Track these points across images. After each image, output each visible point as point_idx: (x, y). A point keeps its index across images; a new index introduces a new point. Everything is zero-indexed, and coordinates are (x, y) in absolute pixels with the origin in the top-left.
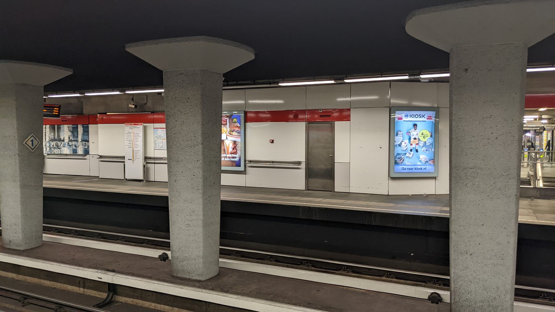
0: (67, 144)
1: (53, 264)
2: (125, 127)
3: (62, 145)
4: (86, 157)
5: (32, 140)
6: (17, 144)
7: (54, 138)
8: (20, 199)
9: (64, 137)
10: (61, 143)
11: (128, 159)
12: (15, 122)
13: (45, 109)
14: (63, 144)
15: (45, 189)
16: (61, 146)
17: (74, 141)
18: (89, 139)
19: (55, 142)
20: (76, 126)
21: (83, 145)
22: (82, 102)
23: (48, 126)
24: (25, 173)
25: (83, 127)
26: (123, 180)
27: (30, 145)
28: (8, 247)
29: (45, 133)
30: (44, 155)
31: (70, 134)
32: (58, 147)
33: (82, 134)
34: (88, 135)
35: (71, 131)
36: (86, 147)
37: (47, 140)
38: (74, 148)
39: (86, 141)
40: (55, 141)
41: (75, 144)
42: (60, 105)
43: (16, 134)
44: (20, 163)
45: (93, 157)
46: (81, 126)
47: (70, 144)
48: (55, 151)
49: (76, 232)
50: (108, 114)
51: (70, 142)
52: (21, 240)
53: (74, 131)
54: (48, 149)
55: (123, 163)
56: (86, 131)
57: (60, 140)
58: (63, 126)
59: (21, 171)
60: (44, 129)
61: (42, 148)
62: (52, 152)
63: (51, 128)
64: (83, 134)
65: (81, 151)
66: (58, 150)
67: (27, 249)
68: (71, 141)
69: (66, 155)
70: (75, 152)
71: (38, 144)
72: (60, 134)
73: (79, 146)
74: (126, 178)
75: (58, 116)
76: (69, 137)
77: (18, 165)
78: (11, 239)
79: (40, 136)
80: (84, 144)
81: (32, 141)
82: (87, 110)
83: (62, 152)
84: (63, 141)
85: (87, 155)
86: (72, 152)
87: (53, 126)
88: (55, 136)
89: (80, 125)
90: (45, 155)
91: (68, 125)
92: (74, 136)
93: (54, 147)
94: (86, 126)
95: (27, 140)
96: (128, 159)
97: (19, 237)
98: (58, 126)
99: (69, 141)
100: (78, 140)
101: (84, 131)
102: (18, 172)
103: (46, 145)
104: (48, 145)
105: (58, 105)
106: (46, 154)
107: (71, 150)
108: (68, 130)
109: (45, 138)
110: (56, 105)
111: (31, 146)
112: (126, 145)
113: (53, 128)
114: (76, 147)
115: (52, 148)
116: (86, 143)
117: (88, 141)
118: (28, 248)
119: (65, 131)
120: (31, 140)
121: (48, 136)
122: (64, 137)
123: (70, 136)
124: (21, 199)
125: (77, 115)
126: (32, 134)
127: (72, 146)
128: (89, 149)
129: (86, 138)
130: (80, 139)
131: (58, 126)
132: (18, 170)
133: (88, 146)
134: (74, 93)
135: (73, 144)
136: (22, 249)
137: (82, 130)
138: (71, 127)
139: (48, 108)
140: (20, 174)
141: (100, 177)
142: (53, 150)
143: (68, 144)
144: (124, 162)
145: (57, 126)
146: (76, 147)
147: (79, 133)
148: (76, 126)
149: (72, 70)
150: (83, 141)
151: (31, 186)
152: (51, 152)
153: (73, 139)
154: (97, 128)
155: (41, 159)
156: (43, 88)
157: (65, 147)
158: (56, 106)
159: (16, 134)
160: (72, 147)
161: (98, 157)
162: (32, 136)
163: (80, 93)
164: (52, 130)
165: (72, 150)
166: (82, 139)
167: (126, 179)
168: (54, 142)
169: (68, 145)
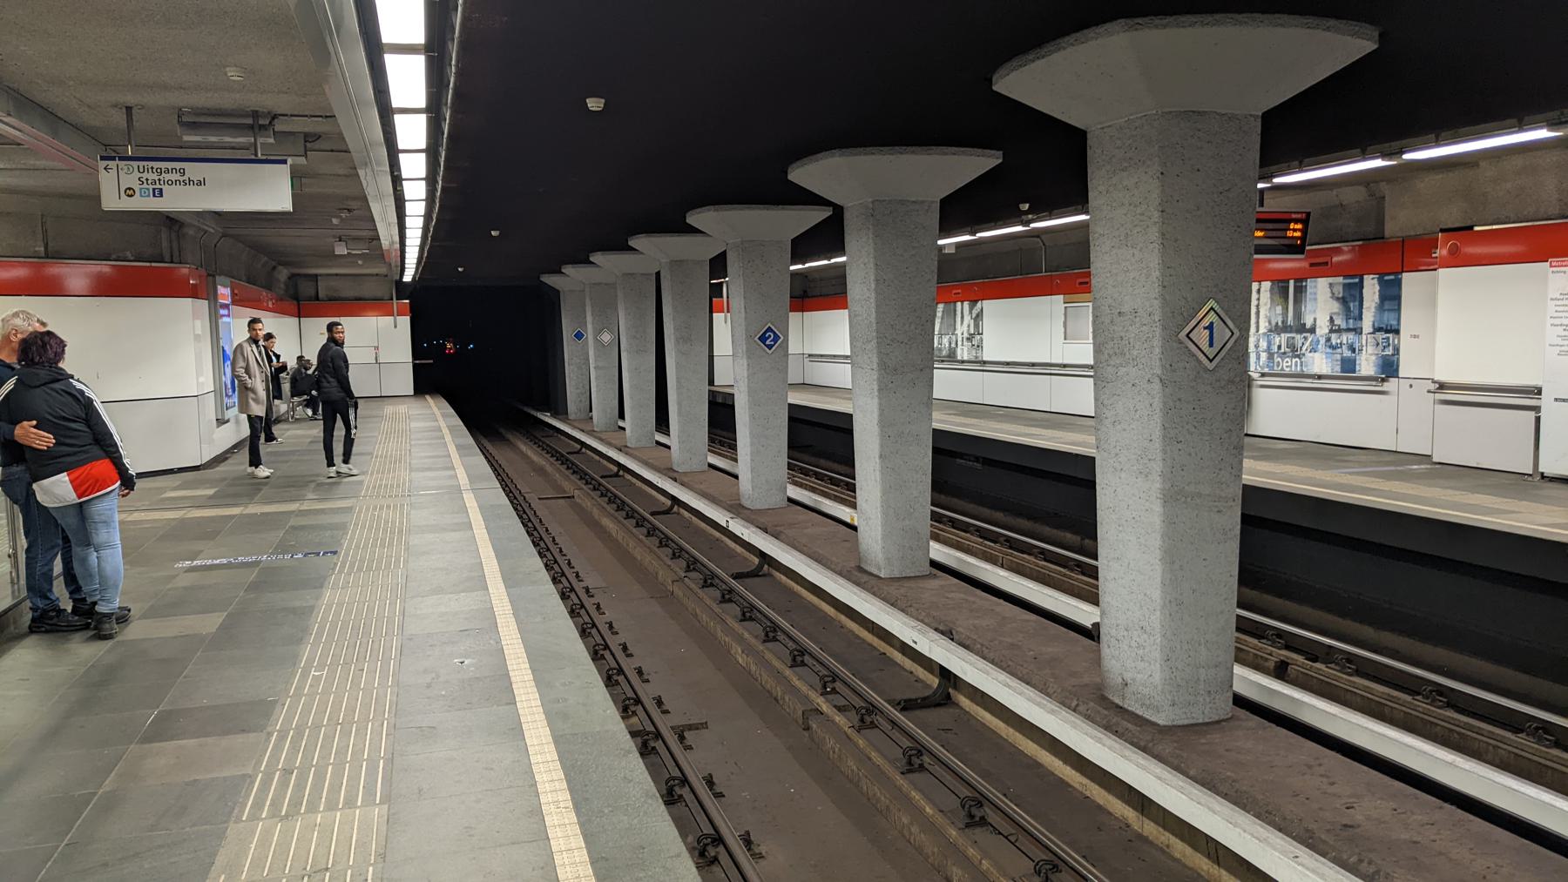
0: (1322, 341)
1: (1265, 841)
2: (1551, 275)
3: (1307, 344)
4: (1386, 387)
5: (1212, 323)
6: (1157, 342)
7: (1283, 322)
8: (1158, 543)
9: (1315, 320)
10: (1306, 338)
11: (1556, 400)
12: (1154, 260)
13: (1261, 230)
14: (1310, 339)
15: (1250, 492)
16: (1304, 348)
17: (1348, 330)
18: (1399, 324)
19: (1284, 336)
20: (1357, 280)
21: (1378, 344)
22: (1384, 197)
23: (1266, 285)
24: (1180, 446)
25: (1380, 284)
26: (1530, 475)
27: (1205, 345)
28: (1117, 701)
29: (1258, 306)
30: (1250, 376)
31: (1335, 307)
32: (1294, 351)
33: (1376, 307)
34: (1399, 309)
35: (1338, 299)
36: (1389, 351)
37: (1262, 330)
38: (1348, 353)
39: (1387, 331)
40: (1285, 332)
41: (1350, 341)
42: (1308, 214)
43: (1156, 302)
44: (1167, 411)
45: (1411, 386)
46: (1376, 281)
47: (1335, 339)
48: (1285, 364)
49: (1349, 661)
50: (1476, 228)
51: (1334, 336)
52: (1160, 688)
53: (1350, 299)
54: (1264, 356)
55: (1532, 414)
56: (1391, 297)
57: (1302, 329)
58: (1313, 284)
59: (1171, 438)
60: (1254, 296)
61: (1246, 355)
62: (1276, 368)
63: (1276, 290)
64: (1381, 308)
65: (1368, 364)
66: (1294, 360)
67: (1175, 723)
68: (1339, 331)
69: (1320, 377)
70: (1348, 366)
71: (1233, 340)
72: (1303, 309)
73: (1364, 348)
74: (1541, 470)
75: (1299, 249)
76: (1331, 318)
77: (1157, 418)
78: (1128, 676)
79: (1242, 320)
80: (1380, 341)
81: (1210, 327)
82: (1400, 221)
83: (1306, 366)
84: (1313, 330)
85: (1391, 379)
86: (1338, 368)
87: (1280, 284)
88: (1287, 317)
89: (1372, 276)
90: (1255, 375)
91: (1331, 280)
92: (1347, 315)
93: (1282, 351)
94: (1392, 277)
95: (1193, 323)
96: (1556, 400)
97: (1151, 676)
98: (1299, 284)
99: (1331, 331)
100: (1362, 329)
101: (1384, 298)
102: (1157, 444)
103: (1257, 346)
104: (1263, 344)
105: (1298, 213)
106: (1258, 375)
107: (1337, 360)
108: (1330, 295)
109: (1258, 323)
110: (1295, 213)
111: (1205, 347)
112: (1550, 345)
113: (1281, 291)
114: (1354, 351)
115: (1276, 355)
116: (1388, 338)
117: (1397, 332)
118: (1180, 723)
119: (1319, 300)
120: (1206, 322)
121: (1266, 317)
122: (1315, 320)
123: (1335, 313)
124: (1164, 542)
125: (1360, 243)
126: (1212, 303)
127: (1341, 347)
128: (1398, 359)
129: (1389, 319)
130: (1367, 324)
131: (1299, 284)
132: (1157, 433)
133: (1397, 350)
134: (1364, 157)
135: (1345, 342)
136: (1161, 722)
137: (1377, 293)
138: (1340, 283)
139: (1270, 226)
140: (1165, 452)
141: (1435, 459)
142: (1279, 362)
143: (1328, 340)
144: (1537, 409)
145: (1295, 282)
146: (1354, 351)
147: (1366, 304)
148: (1357, 280)
149: (1376, 34)
150: (1377, 330)
151: (1200, 495)
152: (1273, 366)
153: (1344, 326)
154: (1435, 282)
155: (1240, 387)
156: (1260, 120)
157: (1315, 352)
158: (1294, 216)
159: (1156, 302)
160: (1339, 350)
161: (1433, 387)
162: (1212, 308)
163: (1384, 156)
164: (1277, 297)
165: (1339, 363)
166: (1374, 325)
167: (1542, 473)
168: (1282, 335)
169: (1329, 344)
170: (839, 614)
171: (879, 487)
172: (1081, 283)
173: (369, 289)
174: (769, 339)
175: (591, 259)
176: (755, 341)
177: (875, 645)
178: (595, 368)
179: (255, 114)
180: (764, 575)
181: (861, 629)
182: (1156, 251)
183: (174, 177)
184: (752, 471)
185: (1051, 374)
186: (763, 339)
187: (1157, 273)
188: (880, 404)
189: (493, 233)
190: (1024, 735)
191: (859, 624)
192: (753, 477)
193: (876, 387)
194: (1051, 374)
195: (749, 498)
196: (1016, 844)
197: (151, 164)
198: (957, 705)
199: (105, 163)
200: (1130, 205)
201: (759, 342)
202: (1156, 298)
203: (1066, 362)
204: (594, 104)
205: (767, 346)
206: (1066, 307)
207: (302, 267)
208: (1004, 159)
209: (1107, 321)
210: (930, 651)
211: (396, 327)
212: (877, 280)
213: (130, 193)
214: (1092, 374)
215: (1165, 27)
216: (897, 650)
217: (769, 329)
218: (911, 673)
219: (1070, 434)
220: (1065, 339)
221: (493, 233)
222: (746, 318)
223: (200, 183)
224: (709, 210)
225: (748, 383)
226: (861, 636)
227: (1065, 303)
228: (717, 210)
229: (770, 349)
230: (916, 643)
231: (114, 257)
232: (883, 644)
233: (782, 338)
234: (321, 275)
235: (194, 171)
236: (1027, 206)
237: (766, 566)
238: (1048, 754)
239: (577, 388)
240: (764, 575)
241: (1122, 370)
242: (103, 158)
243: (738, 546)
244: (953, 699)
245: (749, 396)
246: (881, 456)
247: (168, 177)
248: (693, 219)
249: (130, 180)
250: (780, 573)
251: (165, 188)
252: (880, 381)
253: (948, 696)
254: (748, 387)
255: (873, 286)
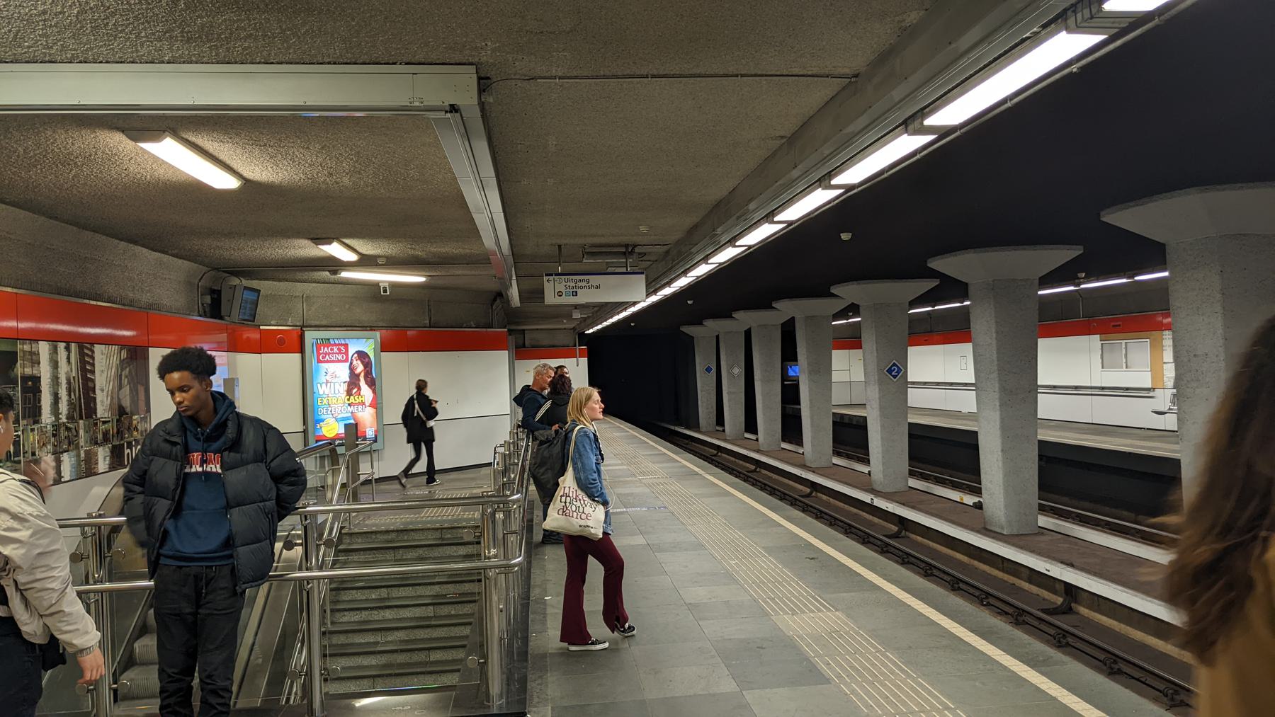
12: (1218, 323)
43: (1220, 349)
170: (972, 561)
171: (1001, 472)
172: (1114, 326)
173: (562, 339)
174: (895, 372)
175: (733, 316)
176: (885, 373)
177: (1006, 579)
178: (728, 393)
179: (627, 246)
180: (902, 537)
181: (992, 569)
182: (1220, 318)
183: (584, 284)
184: (883, 465)
185: (1091, 395)
186: (890, 371)
187: (1221, 331)
188: (1001, 415)
189: (689, 302)
190: (1133, 628)
191: (989, 565)
192: (884, 469)
193: (998, 404)
194: (1091, 395)
195: (881, 483)
196: (1147, 682)
197: (571, 277)
198: (1078, 613)
199: (548, 277)
200: (1200, 289)
201: (888, 374)
202: (1221, 347)
203: (1103, 385)
204: (845, 236)
205: (893, 376)
206: (1102, 344)
207: (518, 325)
208: (1084, 251)
209: (1186, 360)
210: (1061, 575)
211: (578, 365)
212: (997, 332)
213: (560, 294)
214: (974, 388)
215: (1224, 190)
216: (1025, 581)
217: (894, 364)
218: (1038, 595)
219: (1117, 439)
220: (1103, 368)
221: (689, 302)
222: (877, 356)
223: (597, 287)
224: (853, 284)
225: (880, 402)
226: (993, 574)
227: (1101, 341)
228: (859, 284)
229: (895, 378)
230: (1049, 571)
231: (465, 325)
232: (1012, 578)
233: (903, 370)
234: (527, 330)
235: (594, 280)
236: (1084, 275)
237: (904, 531)
238: (1153, 638)
239: (708, 409)
240: (902, 537)
241: (1198, 391)
242: (546, 275)
243: (875, 518)
244: (1074, 610)
245: (880, 411)
246: (1002, 451)
247: (580, 284)
248: (834, 290)
249: (560, 287)
250: (915, 534)
251: (579, 291)
252: (1000, 399)
253: (1071, 609)
254: (880, 405)
255: (994, 335)
